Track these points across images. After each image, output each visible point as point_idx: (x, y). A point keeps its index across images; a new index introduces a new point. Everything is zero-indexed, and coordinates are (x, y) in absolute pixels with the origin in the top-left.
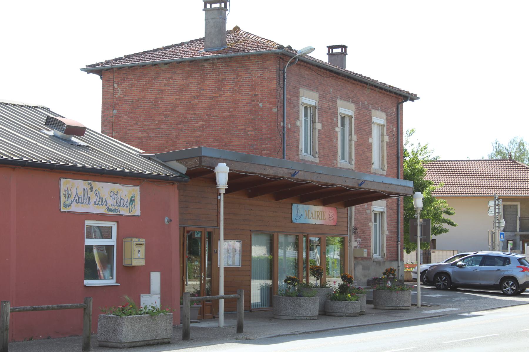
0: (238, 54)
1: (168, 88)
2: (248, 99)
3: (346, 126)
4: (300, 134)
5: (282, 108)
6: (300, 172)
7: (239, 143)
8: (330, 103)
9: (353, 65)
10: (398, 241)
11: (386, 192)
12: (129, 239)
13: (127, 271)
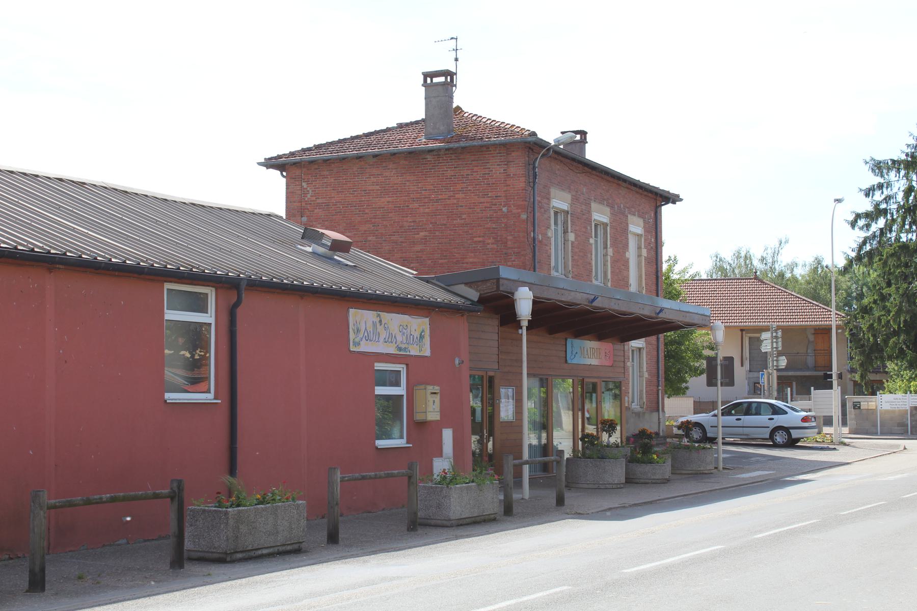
0: (475, 143)
1: (378, 187)
7: (475, 260)
8: (584, 207)
9: (593, 153)
12: (423, 387)
13: (421, 429)
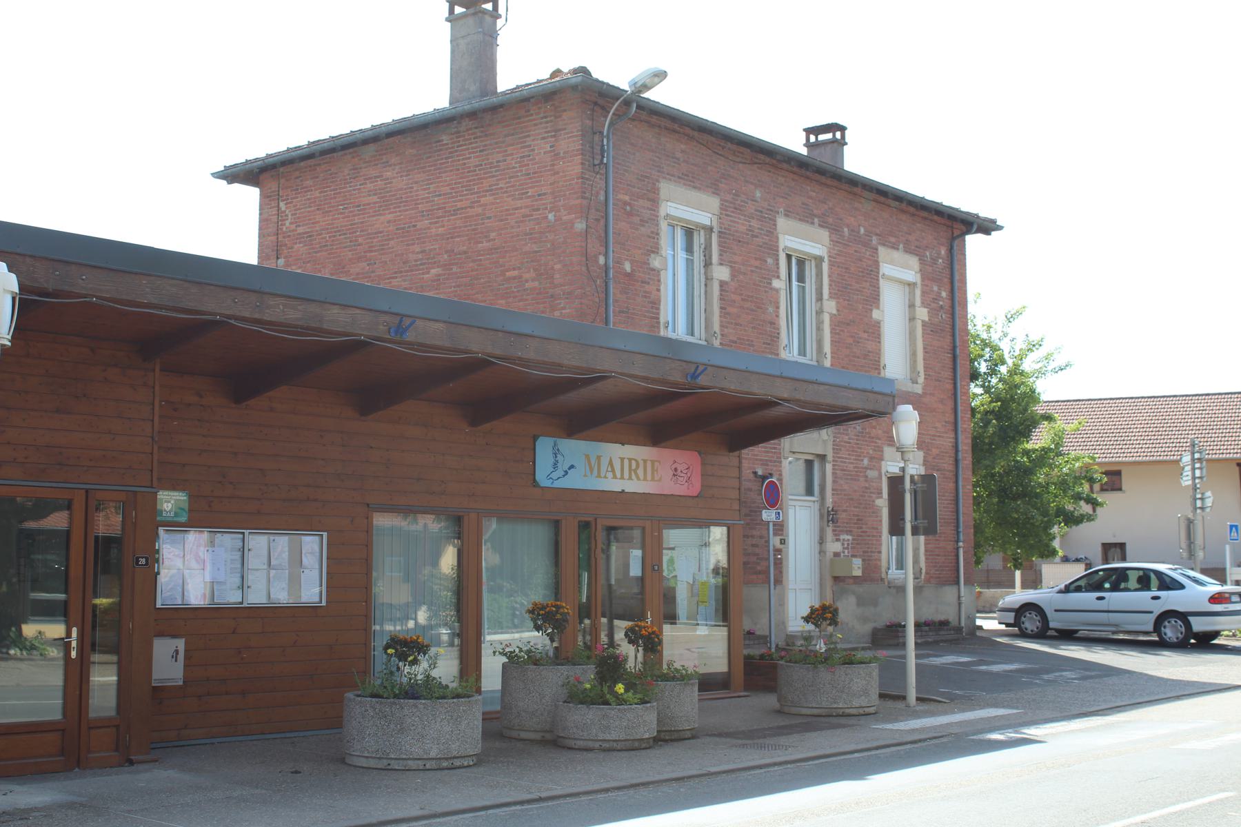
1: (375, 198)
2: (527, 207)
3: (807, 280)
4: (662, 288)
5: (602, 222)
6: (418, 322)
8: (754, 223)
9: (855, 162)
10: (957, 541)
11: (832, 407)
